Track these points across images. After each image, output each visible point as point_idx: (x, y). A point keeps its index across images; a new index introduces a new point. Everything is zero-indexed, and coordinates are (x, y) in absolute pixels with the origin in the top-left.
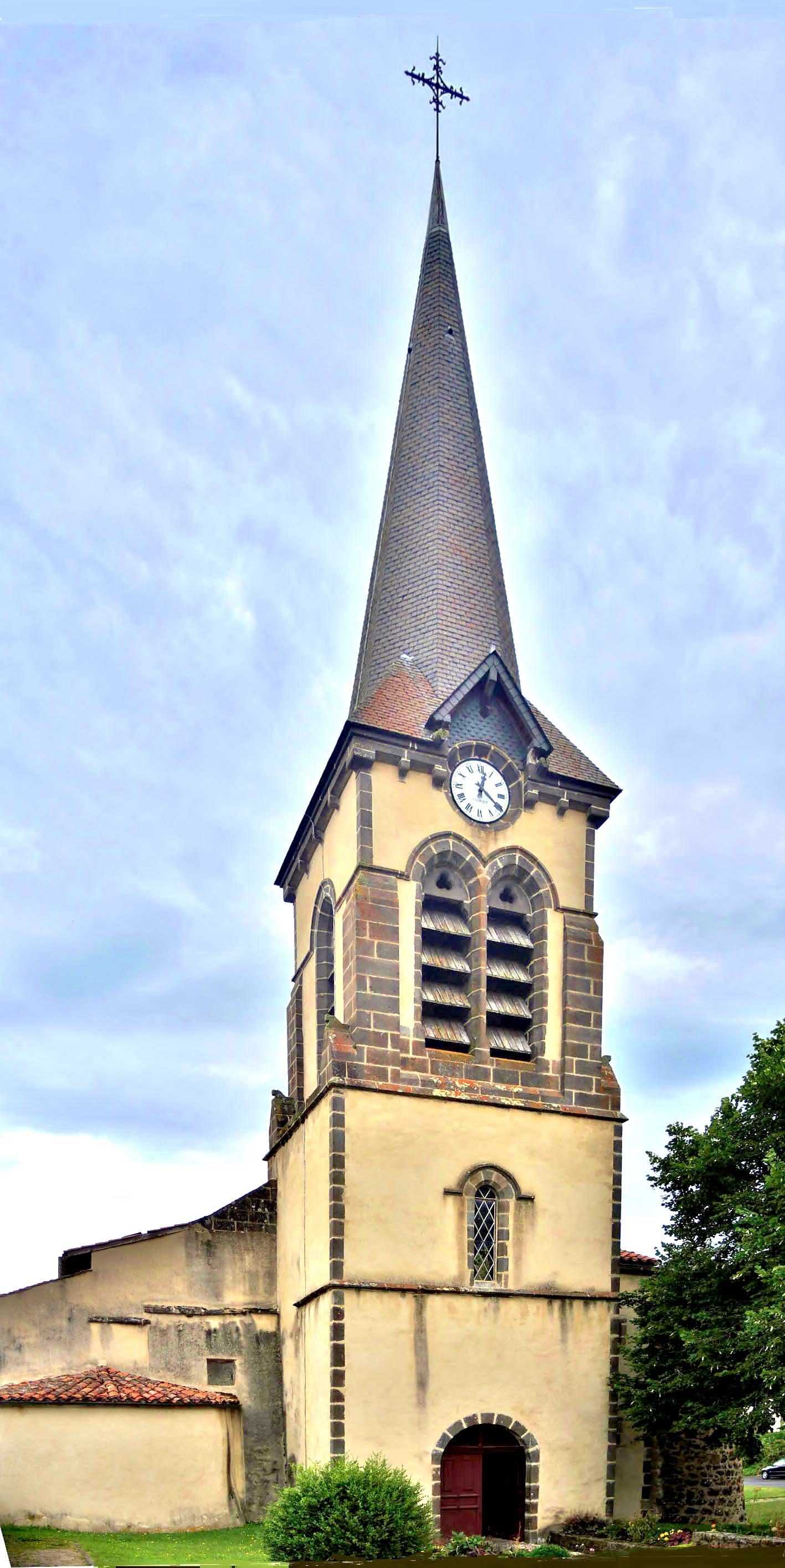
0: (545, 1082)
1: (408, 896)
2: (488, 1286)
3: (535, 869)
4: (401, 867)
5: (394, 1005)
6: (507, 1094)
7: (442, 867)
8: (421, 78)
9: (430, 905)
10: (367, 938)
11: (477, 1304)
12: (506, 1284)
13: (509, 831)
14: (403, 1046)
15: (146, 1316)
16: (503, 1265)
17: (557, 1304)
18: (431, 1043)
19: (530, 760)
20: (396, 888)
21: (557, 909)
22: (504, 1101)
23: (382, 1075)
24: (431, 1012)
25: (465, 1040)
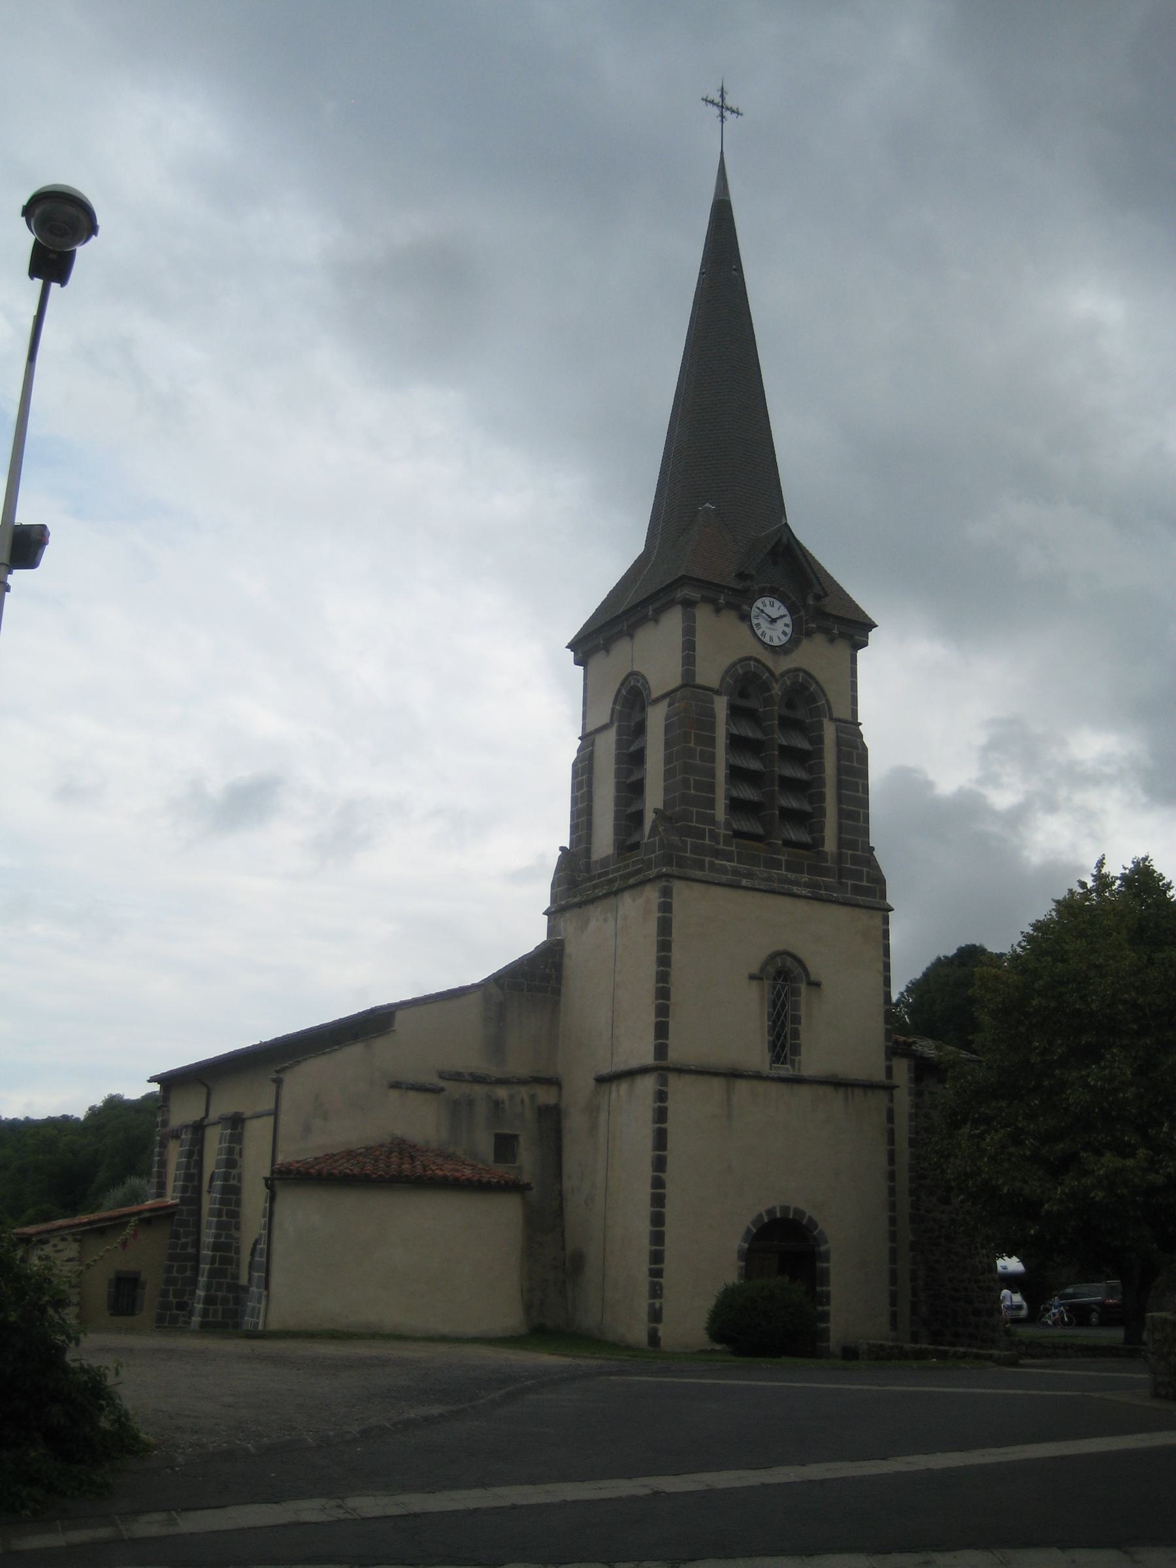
0: (824, 872)
1: (721, 706)
2: (785, 1070)
3: (814, 686)
4: (715, 684)
5: (711, 803)
6: (797, 883)
7: (747, 682)
8: (712, 102)
9: (735, 712)
10: (692, 745)
11: (774, 1089)
12: (799, 1070)
13: (793, 655)
14: (714, 836)
15: (442, 1084)
16: (796, 1050)
17: (841, 1091)
18: (738, 834)
19: (811, 602)
20: (713, 703)
21: (831, 719)
22: (795, 890)
23: (701, 865)
24: (736, 805)
25: (760, 831)
